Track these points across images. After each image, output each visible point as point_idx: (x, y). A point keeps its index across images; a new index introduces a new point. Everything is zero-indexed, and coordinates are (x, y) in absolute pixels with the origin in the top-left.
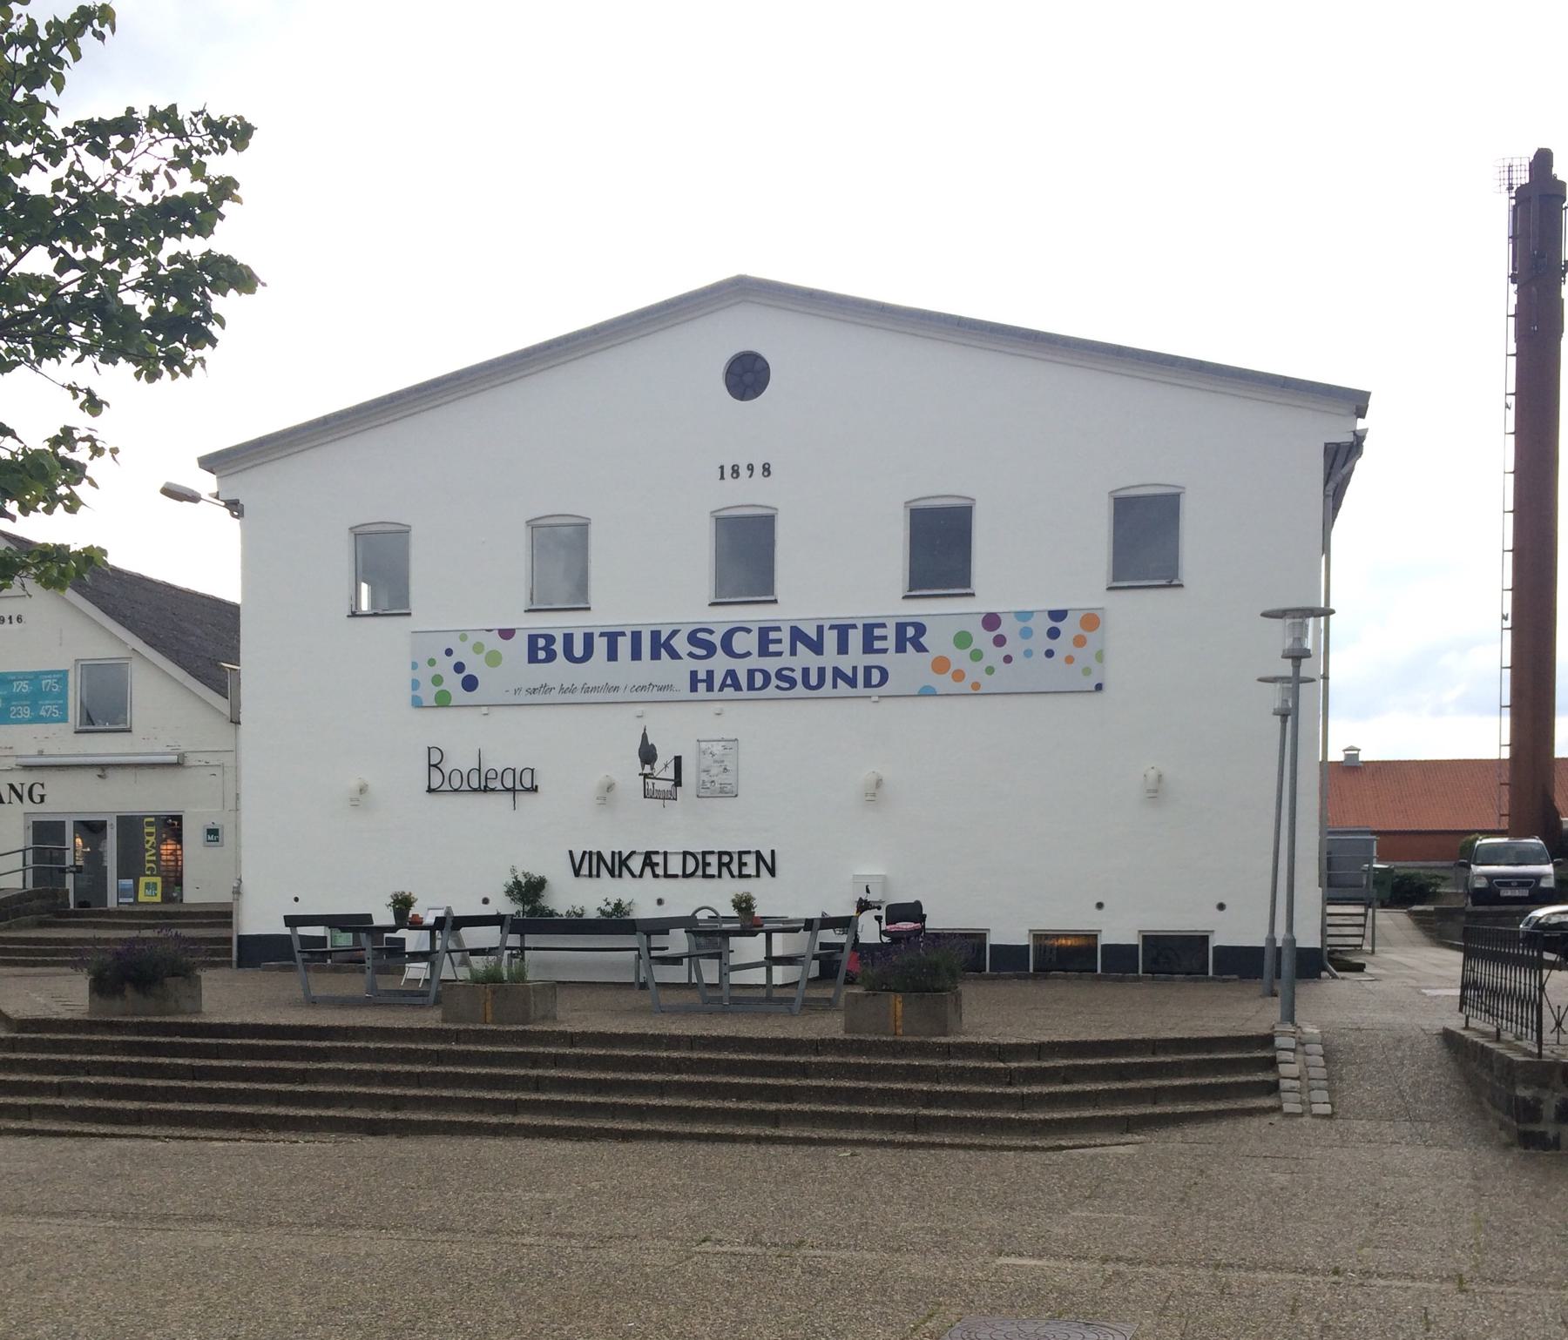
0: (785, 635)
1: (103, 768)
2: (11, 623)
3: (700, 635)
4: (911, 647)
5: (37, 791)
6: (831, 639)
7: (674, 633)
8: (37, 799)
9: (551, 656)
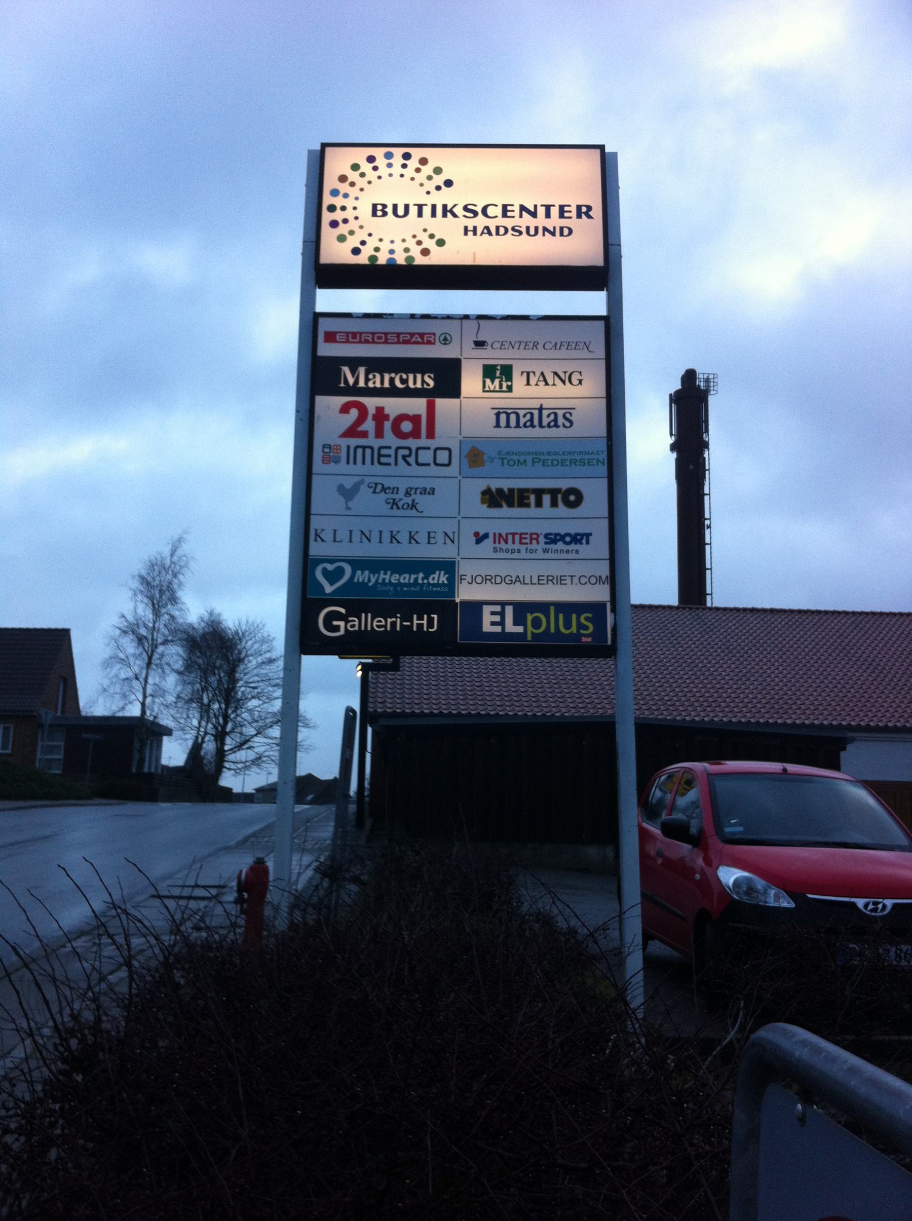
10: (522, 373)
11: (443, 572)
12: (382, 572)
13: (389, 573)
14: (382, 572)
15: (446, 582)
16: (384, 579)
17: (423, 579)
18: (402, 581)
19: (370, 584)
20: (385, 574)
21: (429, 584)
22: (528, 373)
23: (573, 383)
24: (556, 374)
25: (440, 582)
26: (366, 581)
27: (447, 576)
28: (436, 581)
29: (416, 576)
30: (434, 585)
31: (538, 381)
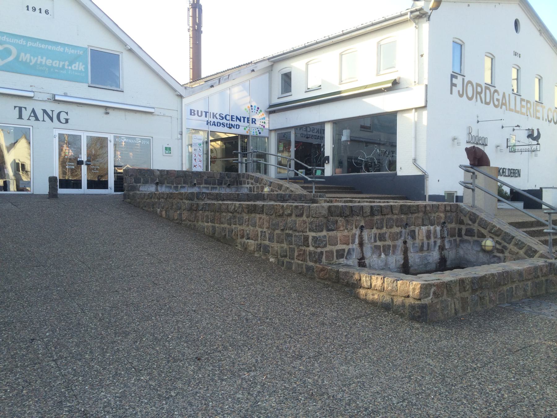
0: (235, 117)
1: (107, 109)
2: (40, 12)
3: (221, 115)
4: (365, 99)
5: (63, 116)
6: (242, 119)
7: (217, 114)
8: (64, 121)
9: (194, 115)
10: (15, 107)
11: (81, 64)
12: (40, 57)
13: (45, 58)
14: (40, 57)
15: (83, 70)
16: (41, 62)
17: (68, 66)
18: (54, 65)
19: (31, 64)
20: (42, 58)
21: (72, 69)
22: (20, 109)
23: (61, 121)
24: (45, 111)
25: (80, 69)
26: (28, 61)
27: (84, 66)
28: (76, 69)
29: (63, 63)
30: (75, 71)
31: (30, 116)
